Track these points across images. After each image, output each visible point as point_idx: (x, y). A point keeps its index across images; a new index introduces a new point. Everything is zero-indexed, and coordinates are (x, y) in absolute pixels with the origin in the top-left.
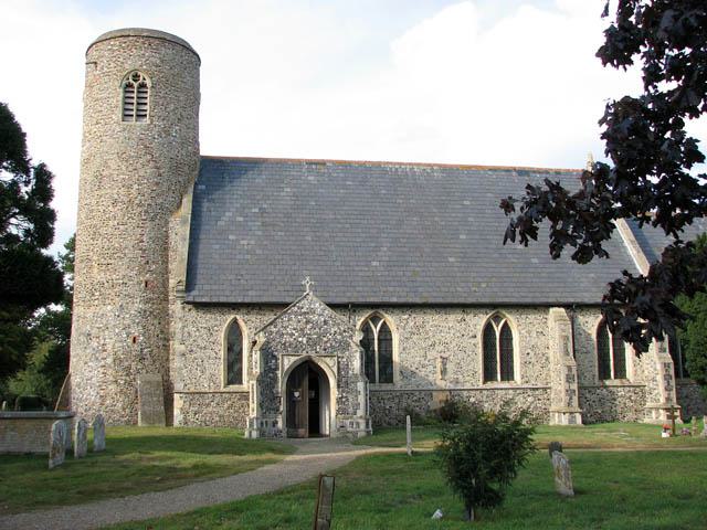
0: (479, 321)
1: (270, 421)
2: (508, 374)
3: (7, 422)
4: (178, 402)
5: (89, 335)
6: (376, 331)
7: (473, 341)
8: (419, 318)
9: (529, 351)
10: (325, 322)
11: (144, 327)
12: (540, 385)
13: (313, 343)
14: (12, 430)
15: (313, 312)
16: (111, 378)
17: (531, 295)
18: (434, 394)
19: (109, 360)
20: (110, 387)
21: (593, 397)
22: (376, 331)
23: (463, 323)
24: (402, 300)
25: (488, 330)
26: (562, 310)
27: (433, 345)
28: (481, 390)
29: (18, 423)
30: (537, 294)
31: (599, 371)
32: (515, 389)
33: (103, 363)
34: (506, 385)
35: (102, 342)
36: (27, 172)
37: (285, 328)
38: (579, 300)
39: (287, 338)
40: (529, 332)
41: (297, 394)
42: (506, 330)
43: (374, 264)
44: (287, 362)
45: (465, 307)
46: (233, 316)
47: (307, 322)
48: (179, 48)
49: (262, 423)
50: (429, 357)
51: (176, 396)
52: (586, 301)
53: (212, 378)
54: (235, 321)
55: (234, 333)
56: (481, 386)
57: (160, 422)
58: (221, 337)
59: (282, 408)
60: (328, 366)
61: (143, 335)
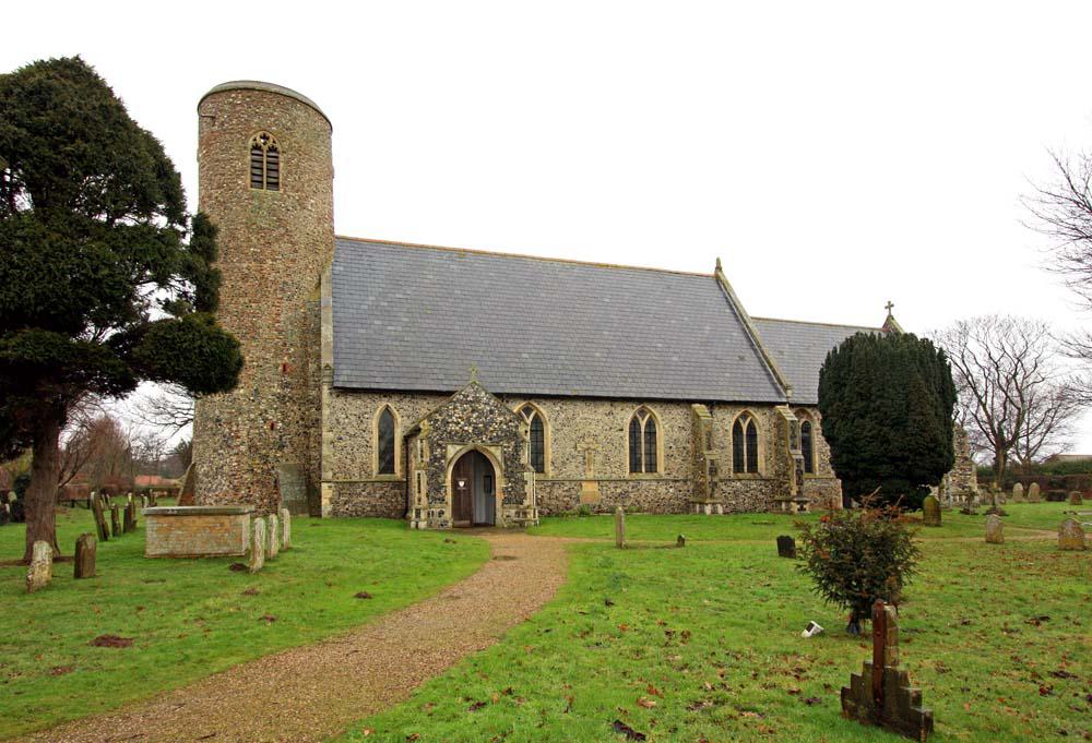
0: (626, 415)
1: (436, 511)
2: (652, 467)
3: (172, 519)
4: (327, 492)
5: (218, 420)
6: (643, 424)
7: (621, 434)
8: (569, 409)
9: (671, 445)
10: (491, 412)
11: (283, 413)
12: (681, 477)
13: (479, 433)
14: (179, 528)
15: (477, 400)
16: (246, 467)
17: (674, 391)
18: (584, 484)
19: (243, 448)
20: (245, 476)
21: (728, 490)
22: (643, 424)
23: (611, 417)
24: (554, 393)
25: (635, 423)
26: (703, 406)
27: (583, 437)
28: (627, 481)
29: (186, 520)
30: (680, 391)
31: (734, 466)
32: (658, 481)
33: (236, 451)
34: (650, 476)
35: (234, 428)
36: (183, 222)
37: (451, 416)
38: (718, 398)
39: (452, 427)
40: (672, 427)
41: (462, 484)
42: (651, 424)
43: (524, 355)
44: (453, 451)
45: (612, 400)
46: (384, 404)
47: (473, 411)
48: (311, 112)
49: (429, 514)
50: (579, 449)
51: (325, 486)
52: (725, 398)
53: (364, 467)
54: (387, 408)
55: (387, 421)
56: (627, 475)
57: (303, 512)
58: (374, 424)
59: (449, 498)
60: (496, 453)
61: (282, 422)
